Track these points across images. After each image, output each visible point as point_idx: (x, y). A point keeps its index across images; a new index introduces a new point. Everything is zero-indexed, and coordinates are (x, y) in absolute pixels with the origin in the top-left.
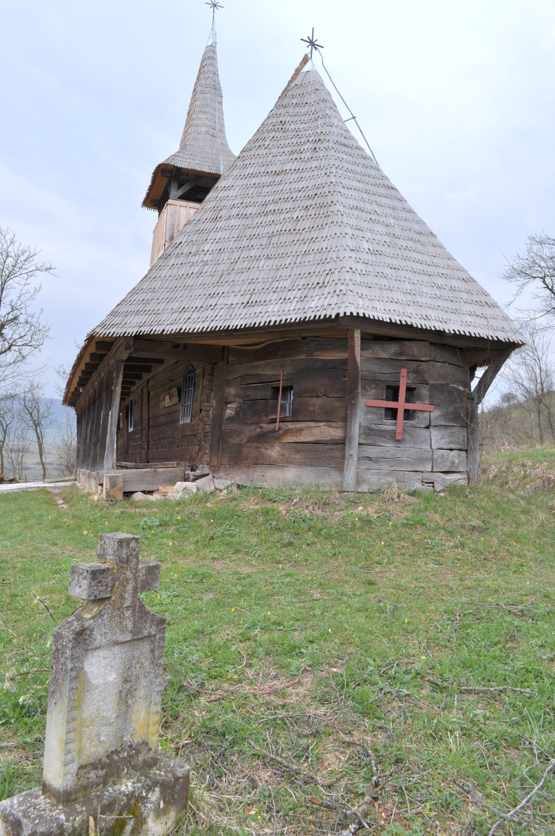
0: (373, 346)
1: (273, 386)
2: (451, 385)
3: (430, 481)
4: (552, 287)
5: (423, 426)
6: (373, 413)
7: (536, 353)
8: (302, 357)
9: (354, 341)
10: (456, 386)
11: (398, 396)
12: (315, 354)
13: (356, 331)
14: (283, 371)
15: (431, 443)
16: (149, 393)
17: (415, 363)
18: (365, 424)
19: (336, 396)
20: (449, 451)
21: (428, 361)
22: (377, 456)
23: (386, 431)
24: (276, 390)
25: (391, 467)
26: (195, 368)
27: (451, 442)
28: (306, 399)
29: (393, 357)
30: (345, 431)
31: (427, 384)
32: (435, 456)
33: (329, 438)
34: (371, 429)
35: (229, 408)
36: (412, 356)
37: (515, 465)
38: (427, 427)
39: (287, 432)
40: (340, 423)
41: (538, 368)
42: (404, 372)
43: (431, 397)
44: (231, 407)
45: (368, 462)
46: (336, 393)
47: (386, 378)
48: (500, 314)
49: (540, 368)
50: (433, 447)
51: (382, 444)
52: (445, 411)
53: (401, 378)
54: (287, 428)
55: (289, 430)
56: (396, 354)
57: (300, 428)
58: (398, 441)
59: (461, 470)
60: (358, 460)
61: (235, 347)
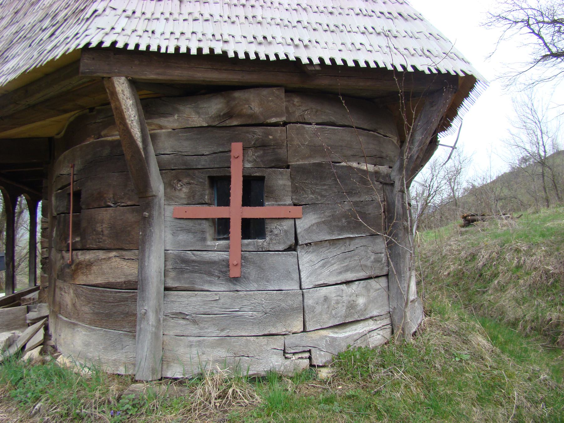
0: (181, 108)
2: (343, 164)
3: (301, 349)
4: (539, 31)
6: (189, 231)
7: (535, 116)
8: (92, 140)
9: (118, 100)
11: (229, 195)
12: (103, 133)
17: (259, 131)
20: (344, 287)
21: (285, 124)
22: (195, 310)
23: (212, 263)
25: (222, 330)
27: (347, 269)
29: (215, 123)
31: (288, 167)
32: (309, 302)
33: (122, 280)
34: (185, 261)
36: (250, 116)
37: (508, 249)
38: (292, 248)
41: (539, 130)
42: (237, 148)
43: (295, 190)
45: (182, 322)
47: (203, 162)
48: (423, 29)
49: (541, 131)
51: (206, 287)
53: (232, 160)
56: (220, 116)
57: (89, 261)
58: (235, 280)
59: (375, 313)
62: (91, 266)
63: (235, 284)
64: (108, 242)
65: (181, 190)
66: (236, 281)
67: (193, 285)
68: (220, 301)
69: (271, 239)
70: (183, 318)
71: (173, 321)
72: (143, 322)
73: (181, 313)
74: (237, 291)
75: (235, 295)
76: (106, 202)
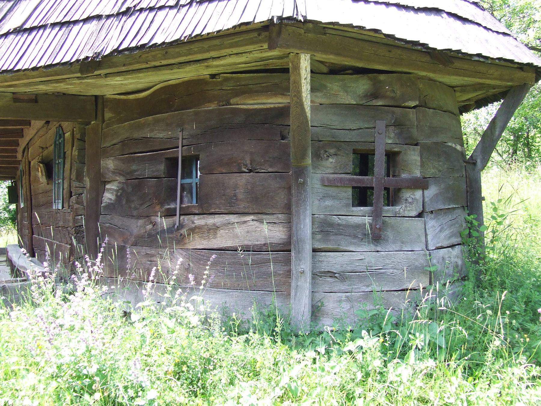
1: (168, 156)
2: (450, 144)
5: (414, 213)
10: (454, 145)
12: (232, 101)
13: (303, 56)
14: (182, 130)
15: (427, 241)
16: (30, 163)
18: (322, 216)
19: (270, 170)
24: (172, 162)
26: (65, 132)
28: (221, 176)
30: (290, 229)
31: (416, 145)
35: (108, 189)
36: (393, 98)
38: (420, 215)
39: (193, 230)
40: (280, 216)
44: (110, 189)
45: (329, 279)
46: (271, 166)
50: (431, 247)
52: (442, 186)
54: (193, 226)
55: (196, 227)
57: (214, 225)
60: (313, 278)
61: (118, 97)
62: (216, 230)
63: (376, 246)
64: (242, 206)
65: (327, 160)
66: (377, 243)
67: (338, 247)
68: (365, 260)
69: (406, 207)
70: (331, 277)
71: (321, 279)
72: (299, 280)
73: (328, 271)
74: (378, 251)
75: (378, 255)
76: (240, 168)
